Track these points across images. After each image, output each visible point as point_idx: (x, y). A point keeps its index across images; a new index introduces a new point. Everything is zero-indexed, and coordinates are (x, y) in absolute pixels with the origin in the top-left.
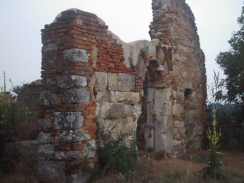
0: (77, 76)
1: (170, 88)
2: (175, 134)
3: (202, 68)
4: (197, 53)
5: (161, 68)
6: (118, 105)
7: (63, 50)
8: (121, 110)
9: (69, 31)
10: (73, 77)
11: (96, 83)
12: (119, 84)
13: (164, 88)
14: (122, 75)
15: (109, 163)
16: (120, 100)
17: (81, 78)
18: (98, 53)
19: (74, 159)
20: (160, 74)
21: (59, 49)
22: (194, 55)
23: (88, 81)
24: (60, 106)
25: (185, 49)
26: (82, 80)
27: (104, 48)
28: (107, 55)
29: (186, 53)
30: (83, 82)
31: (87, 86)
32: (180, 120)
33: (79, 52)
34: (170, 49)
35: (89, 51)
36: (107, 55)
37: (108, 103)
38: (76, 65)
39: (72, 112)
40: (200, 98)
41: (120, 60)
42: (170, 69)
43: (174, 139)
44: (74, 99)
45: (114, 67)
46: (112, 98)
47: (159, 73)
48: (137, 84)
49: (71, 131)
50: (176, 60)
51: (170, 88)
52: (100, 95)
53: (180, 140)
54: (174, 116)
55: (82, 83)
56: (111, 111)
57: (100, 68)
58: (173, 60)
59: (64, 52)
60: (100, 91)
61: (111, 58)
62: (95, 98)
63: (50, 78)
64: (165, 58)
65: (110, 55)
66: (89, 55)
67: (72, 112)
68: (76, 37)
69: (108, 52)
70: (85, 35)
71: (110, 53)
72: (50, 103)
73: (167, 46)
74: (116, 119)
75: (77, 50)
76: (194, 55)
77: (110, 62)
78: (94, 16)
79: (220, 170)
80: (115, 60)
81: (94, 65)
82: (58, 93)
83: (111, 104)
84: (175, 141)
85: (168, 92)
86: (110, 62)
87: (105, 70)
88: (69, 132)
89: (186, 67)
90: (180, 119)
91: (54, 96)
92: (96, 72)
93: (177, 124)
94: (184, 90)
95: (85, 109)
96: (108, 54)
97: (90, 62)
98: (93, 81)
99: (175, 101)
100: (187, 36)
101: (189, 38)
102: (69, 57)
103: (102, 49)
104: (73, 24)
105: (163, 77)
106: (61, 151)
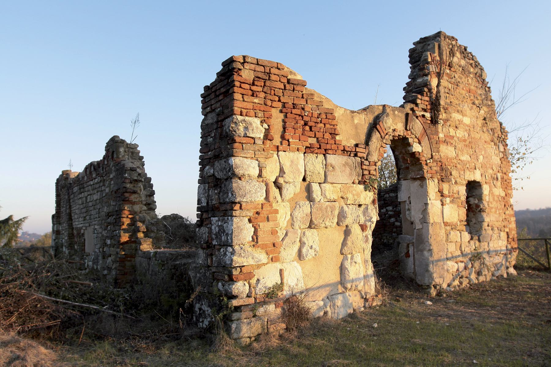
9: (229, 90)
30: (251, 169)
94: (465, 183)
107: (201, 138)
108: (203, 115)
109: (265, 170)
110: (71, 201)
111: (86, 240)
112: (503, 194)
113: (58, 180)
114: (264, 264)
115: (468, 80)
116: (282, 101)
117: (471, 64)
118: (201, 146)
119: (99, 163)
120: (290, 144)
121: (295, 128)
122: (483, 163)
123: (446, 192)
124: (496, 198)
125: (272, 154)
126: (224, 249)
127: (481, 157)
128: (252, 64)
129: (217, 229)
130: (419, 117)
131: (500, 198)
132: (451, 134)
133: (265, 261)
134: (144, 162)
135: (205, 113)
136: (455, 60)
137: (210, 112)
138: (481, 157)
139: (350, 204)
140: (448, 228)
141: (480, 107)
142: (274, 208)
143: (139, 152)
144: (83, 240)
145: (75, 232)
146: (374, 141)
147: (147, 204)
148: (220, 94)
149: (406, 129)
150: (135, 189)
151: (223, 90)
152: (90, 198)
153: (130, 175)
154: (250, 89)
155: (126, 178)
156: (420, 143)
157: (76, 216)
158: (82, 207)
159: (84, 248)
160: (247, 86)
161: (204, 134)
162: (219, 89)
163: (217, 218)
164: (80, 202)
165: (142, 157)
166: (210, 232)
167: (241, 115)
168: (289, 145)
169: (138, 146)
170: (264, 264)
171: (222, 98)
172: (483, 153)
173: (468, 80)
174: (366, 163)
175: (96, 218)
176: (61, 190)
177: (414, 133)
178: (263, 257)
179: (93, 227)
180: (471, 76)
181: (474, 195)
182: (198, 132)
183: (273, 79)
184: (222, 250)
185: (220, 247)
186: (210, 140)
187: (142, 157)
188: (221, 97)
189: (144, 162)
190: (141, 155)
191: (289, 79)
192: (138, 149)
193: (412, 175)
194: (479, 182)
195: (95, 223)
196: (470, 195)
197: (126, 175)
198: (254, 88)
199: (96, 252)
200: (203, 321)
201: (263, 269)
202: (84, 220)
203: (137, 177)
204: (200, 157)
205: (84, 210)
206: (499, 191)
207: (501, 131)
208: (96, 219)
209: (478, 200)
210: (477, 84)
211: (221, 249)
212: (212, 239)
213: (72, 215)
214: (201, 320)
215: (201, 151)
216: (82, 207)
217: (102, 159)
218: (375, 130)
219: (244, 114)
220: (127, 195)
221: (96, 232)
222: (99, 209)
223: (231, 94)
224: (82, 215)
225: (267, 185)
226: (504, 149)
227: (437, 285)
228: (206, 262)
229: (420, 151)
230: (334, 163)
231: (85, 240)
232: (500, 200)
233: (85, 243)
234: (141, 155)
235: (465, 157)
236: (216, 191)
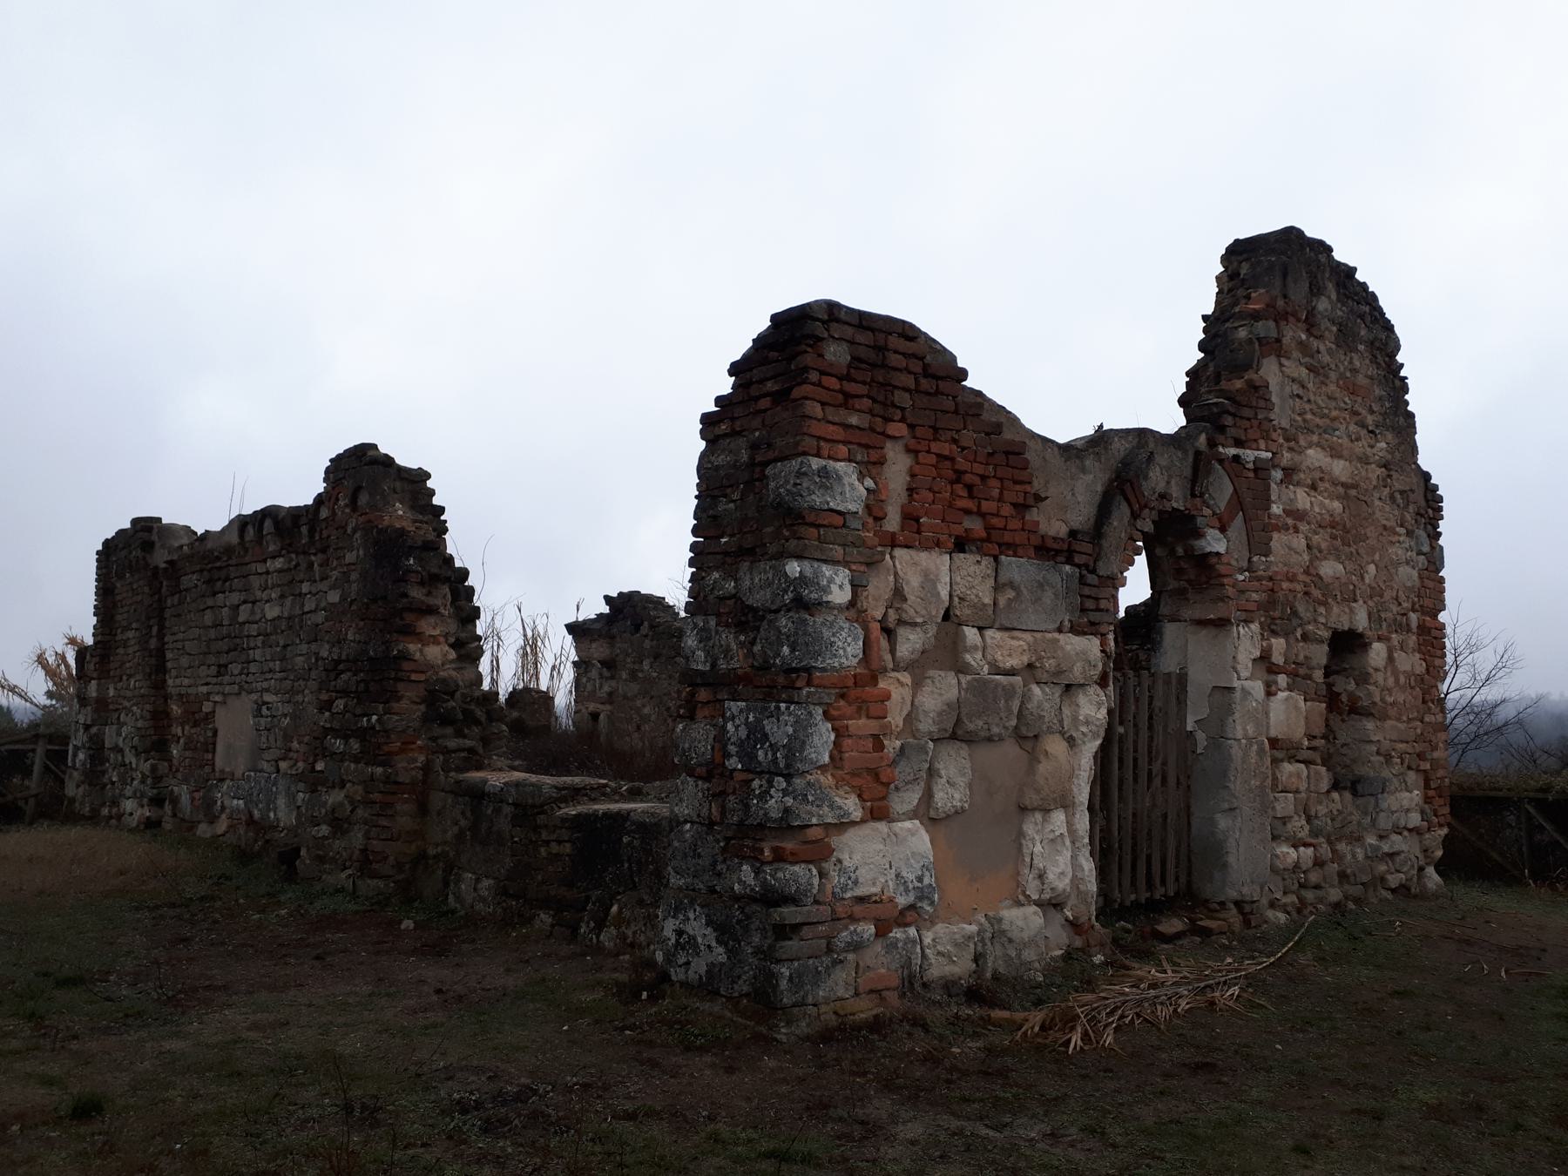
0: (806, 563)
1: (1255, 627)
2: (1284, 820)
3: (1426, 548)
4: (1397, 486)
5: (1215, 542)
6: (998, 684)
7: (768, 463)
8: (1009, 710)
9: (790, 389)
10: (794, 568)
11: (899, 594)
12: (1002, 602)
13: (1222, 623)
14: (1018, 568)
15: (912, 931)
16: (1008, 665)
17: (827, 571)
18: (913, 476)
19: (793, 900)
20: (1212, 567)
21: (752, 464)
22: (1387, 491)
23: (856, 587)
24: (746, 679)
25: (1339, 468)
26: (831, 581)
27: (938, 455)
28: (952, 483)
29: (1343, 485)
30: (834, 588)
31: (852, 604)
32: (1307, 762)
33: (824, 473)
34: (1261, 469)
35: (871, 466)
36: (952, 483)
37: (951, 678)
38: (808, 520)
39: (783, 705)
40: (1408, 675)
41: (1015, 505)
42: (1258, 543)
43: (1275, 838)
44: (793, 650)
45: (984, 535)
46: (968, 657)
47: (1205, 562)
48: (1090, 604)
49: (780, 782)
50: (1287, 512)
51: (1255, 627)
52: (910, 642)
53: (1306, 845)
54: (1274, 743)
55: (826, 590)
56: (964, 711)
57: (913, 533)
58: (1276, 509)
59: (769, 471)
60: (915, 624)
61: (971, 496)
62: (893, 651)
63: (717, 568)
64: (1237, 502)
65: (970, 487)
66: (869, 483)
67: (783, 705)
68: (817, 410)
69: (956, 471)
70: (857, 403)
71: (968, 478)
72: (714, 665)
73: (1249, 455)
74: (990, 739)
75: (816, 463)
76: (1387, 491)
77: (967, 512)
78: (907, 332)
79: (630, 976)
80: (987, 506)
81: (893, 523)
82: (741, 627)
83: (965, 679)
84: (1284, 849)
85: (1246, 642)
86: (967, 512)
87: (938, 544)
88: (770, 784)
89: (1339, 542)
90: (1306, 754)
91: (728, 638)
92: (898, 552)
93: (1291, 775)
94: (1326, 634)
95: (843, 696)
96: (958, 481)
97: (874, 507)
98: (879, 588)
99: (1282, 680)
100: (1356, 413)
101: (1363, 425)
102: (782, 490)
103: (932, 459)
104: (809, 359)
105: (1226, 581)
106: (744, 858)
107: (696, 497)
108: (703, 438)
109: (865, 594)
110: (167, 614)
111: (220, 733)
112: (1420, 668)
113: (107, 543)
114: (853, 823)
115: (1351, 358)
116: (909, 421)
117: (1362, 317)
118: (695, 519)
119: (296, 513)
120: (923, 529)
121: (936, 489)
122: (1374, 585)
123: (1278, 659)
124: (1402, 679)
125: (883, 554)
126: (764, 782)
127: (1372, 568)
128: (846, 327)
129: (743, 733)
130: (1226, 463)
131: (1413, 678)
132: (1300, 506)
133: (857, 814)
134: (446, 521)
135: (711, 437)
136: (1323, 305)
137: (725, 435)
138: (1372, 568)
139: (1046, 683)
140: (1279, 754)
141: (1378, 432)
142: (153, 538)
143: (432, 493)
144: (210, 734)
145: (176, 709)
146: (1115, 523)
147: (457, 645)
148: (765, 396)
149: (1193, 495)
150: (431, 601)
151: (770, 386)
152: (253, 612)
153: (419, 560)
154: (841, 391)
155: (409, 571)
156: (1223, 530)
157: (184, 661)
158: (212, 634)
159: (213, 759)
160: (833, 383)
161: (707, 489)
162: (762, 381)
163: (742, 704)
164: (208, 618)
165: (442, 510)
166: (721, 738)
167: (818, 455)
168: (919, 532)
169: (428, 476)
170: (853, 823)
171: (768, 406)
172: (1377, 557)
173: (1351, 358)
174: (1091, 579)
175: (270, 671)
176: (121, 577)
177: (1212, 502)
178: (852, 805)
179: (254, 697)
180: (1361, 347)
181: (1345, 670)
182: (690, 483)
183: (893, 364)
184: (756, 783)
185: (751, 776)
186: (724, 506)
187: (442, 510)
188: (765, 403)
189: (446, 521)
190: (436, 501)
191: (929, 365)
192: (429, 484)
193: (1197, 612)
194: (1361, 636)
195: (265, 685)
196: (1334, 668)
197: (411, 562)
198: (851, 388)
199: (262, 771)
200: (688, 963)
201: (851, 836)
202: (219, 674)
203: (440, 567)
204: (694, 547)
205: (223, 645)
206: (1409, 662)
207: (1425, 496)
208: (269, 676)
209: (1357, 684)
210: (1372, 371)
211: (754, 780)
212: (727, 755)
213: (169, 655)
214: (682, 960)
215: (696, 531)
216: (212, 634)
217: (310, 502)
218: (1119, 498)
219: (825, 453)
220: (409, 617)
221: (264, 711)
222: (285, 647)
223: (796, 400)
224: (212, 659)
225: (866, 630)
226: (1431, 545)
227: (1243, 902)
228: (705, 812)
229: (1222, 550)
230: (1017, 578)
231: (215, 732)
232: (1413, 683)
233: (214, 744)
234: (436, 501)
235: (1330, 569)
236: (742, 638)
